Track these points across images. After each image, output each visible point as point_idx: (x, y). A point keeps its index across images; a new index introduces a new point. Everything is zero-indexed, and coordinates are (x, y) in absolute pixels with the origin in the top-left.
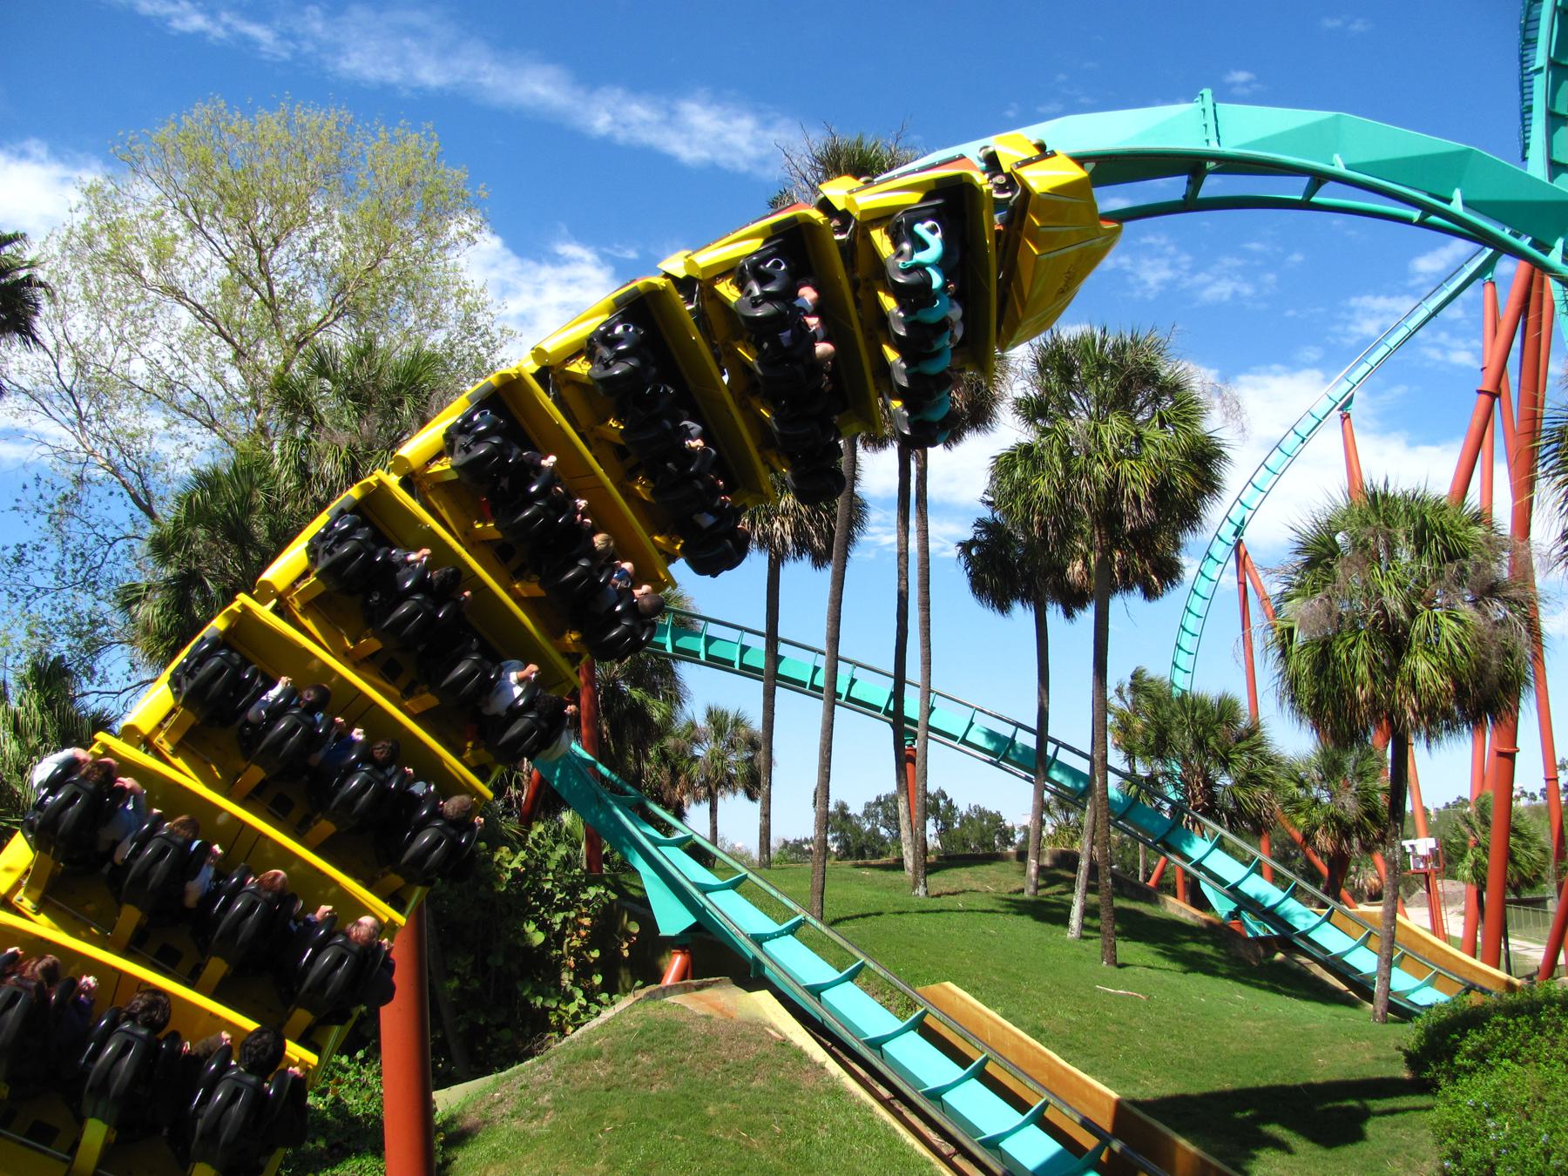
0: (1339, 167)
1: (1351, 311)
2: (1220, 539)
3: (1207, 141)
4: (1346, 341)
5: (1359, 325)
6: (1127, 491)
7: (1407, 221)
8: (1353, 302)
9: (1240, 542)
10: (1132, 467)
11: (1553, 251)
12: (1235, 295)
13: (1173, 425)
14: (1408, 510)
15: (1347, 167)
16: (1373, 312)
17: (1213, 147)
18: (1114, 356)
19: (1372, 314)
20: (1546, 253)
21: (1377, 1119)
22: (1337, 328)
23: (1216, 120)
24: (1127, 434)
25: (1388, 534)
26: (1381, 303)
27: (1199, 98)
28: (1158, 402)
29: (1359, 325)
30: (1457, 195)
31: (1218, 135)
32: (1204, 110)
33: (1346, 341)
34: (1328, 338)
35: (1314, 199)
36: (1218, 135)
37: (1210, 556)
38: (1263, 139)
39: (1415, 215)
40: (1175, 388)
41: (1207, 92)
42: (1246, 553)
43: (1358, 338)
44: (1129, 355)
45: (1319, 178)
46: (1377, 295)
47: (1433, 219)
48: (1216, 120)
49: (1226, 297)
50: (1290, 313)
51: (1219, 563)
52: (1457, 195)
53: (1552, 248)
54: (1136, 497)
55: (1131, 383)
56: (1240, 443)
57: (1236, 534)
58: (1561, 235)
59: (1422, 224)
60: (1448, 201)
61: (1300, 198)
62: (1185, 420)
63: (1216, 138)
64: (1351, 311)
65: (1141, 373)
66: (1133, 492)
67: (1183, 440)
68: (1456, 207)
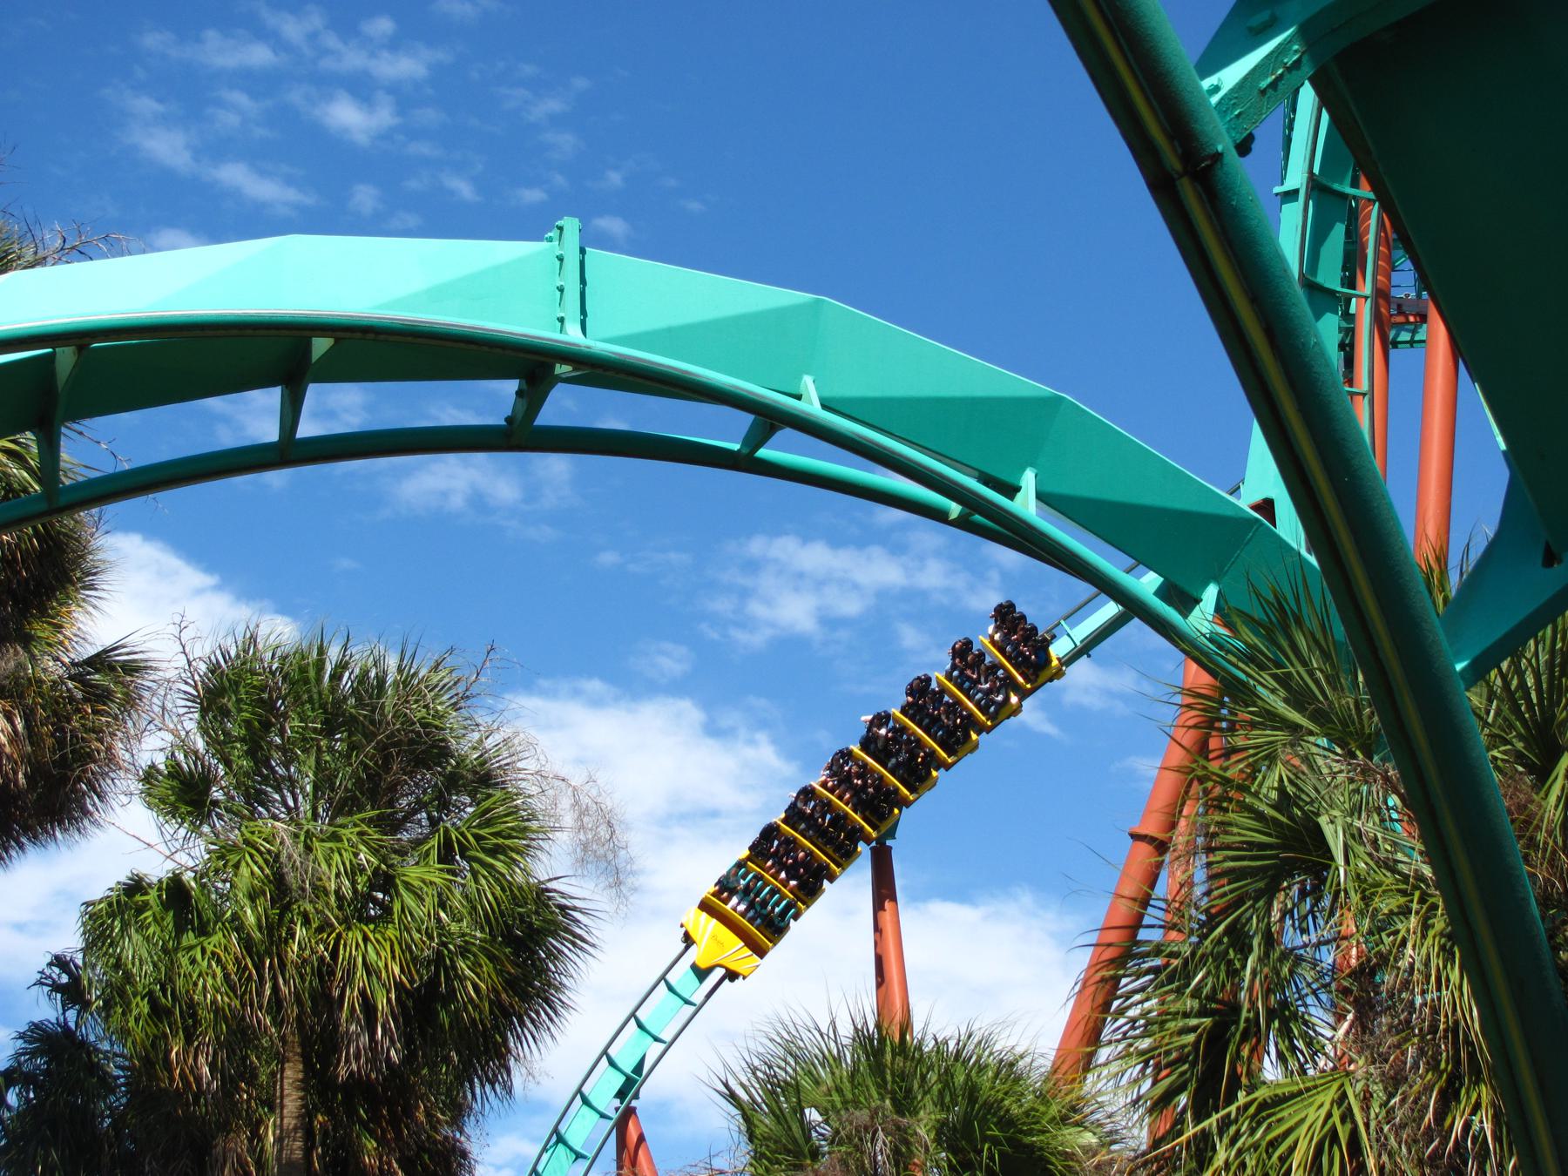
0: (811, 406)
1: (753, 566)
2: (586, 1102)
3: (561, 320)
4: (740, 636)
5: (768, 602)
6: (352, 994)
7: (939, 515)
8: (756, 546)
9: (629, 1113)
10: (366, 939)
11: (1196, 612)
12: (478, 501)
13: (470, 859)
14: (947, 1077)
15: (825, 407)
16: (801, 575)
17: (572, 336)
18: (359, 699)
19: (799, 580)
20: (1185, 613)
21: (1163, 799)
22: (722, 605)
23: (583, 281)
24: (191, 821)
25: (899, 1128)
26: (815, 557)
27: (554, 234)
28: (444, 806)
29: (768, 602)
30: (1028, 481)
31: (583, 312)
32: (561, 259)
33: (740, 636)
34: (704, 626)
35: (764, 453)
36: (583, 312)
37: (561, 1140)
38: (669, 330)
39: (955, 509)
40: (483, 779)
41: (571, 225)
42: (641, 1139)
43: (768, 632)
44: (389, 700)
45: (770, 420)
46: (806, 539)
47: (978, 518)
48: (583, 281)
49: (457, 502)
50: (608, 558)
51: (579, 1156)
52: (1028, 481)
53: (1198, 601)
54: (369, 1008)
55: (387, 759)
56: (610, 908)
57: (621, 1094)
58: (1216, 579)
59: (963, 523)
60: (1011, 491)
61: (736, 447)
62: (494, 851)
63: (578, 317)
64: (753, 566)
65: (411, 742)
66: (363, 993)
67: (489, 891)
68: (1026, 505)
